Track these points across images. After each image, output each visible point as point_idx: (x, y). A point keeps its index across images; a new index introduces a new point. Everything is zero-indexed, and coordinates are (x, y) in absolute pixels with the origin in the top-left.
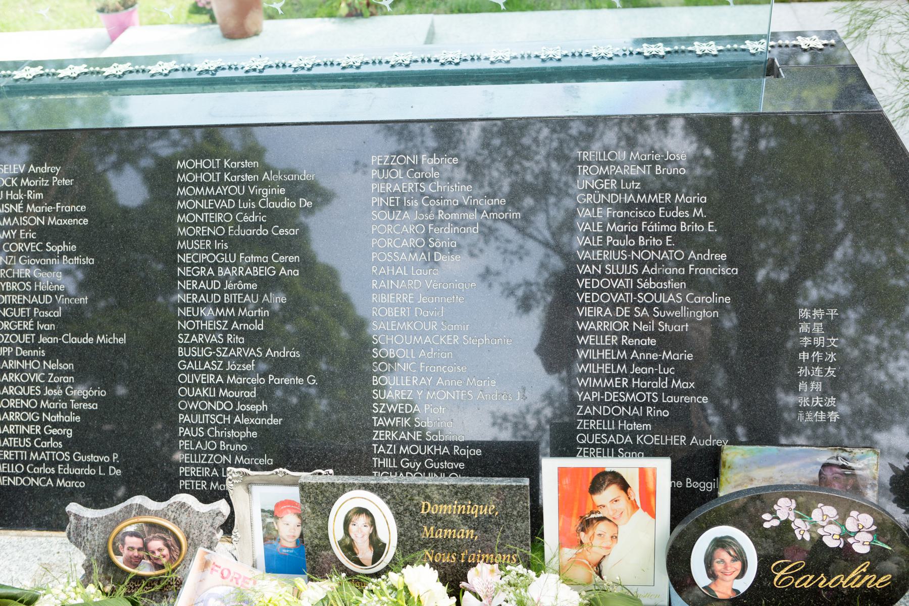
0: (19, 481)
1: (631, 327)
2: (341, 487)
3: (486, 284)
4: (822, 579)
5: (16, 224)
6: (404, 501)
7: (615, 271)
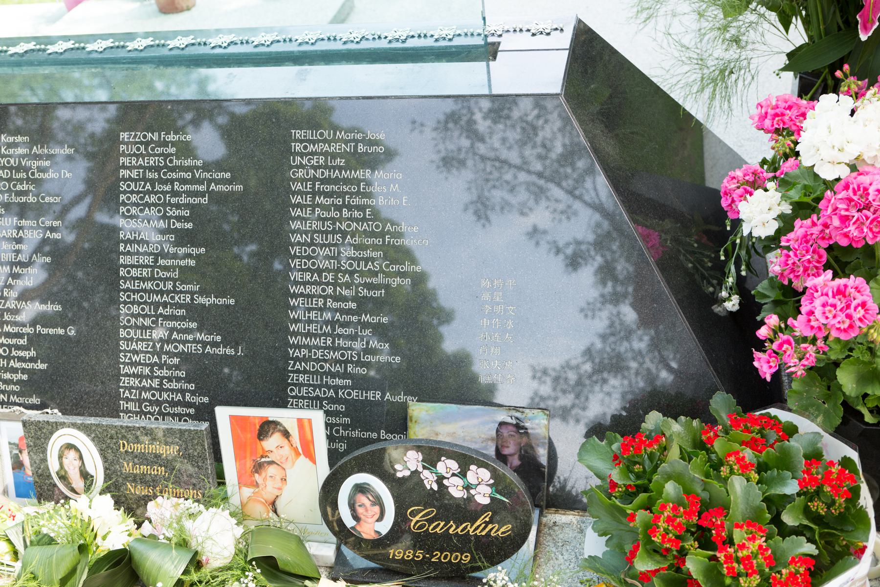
1: (335, 291)
2: (54, 425)
3: (533, 242)
4: (451, 526)
6: (106, 439)
7: (322, 240)
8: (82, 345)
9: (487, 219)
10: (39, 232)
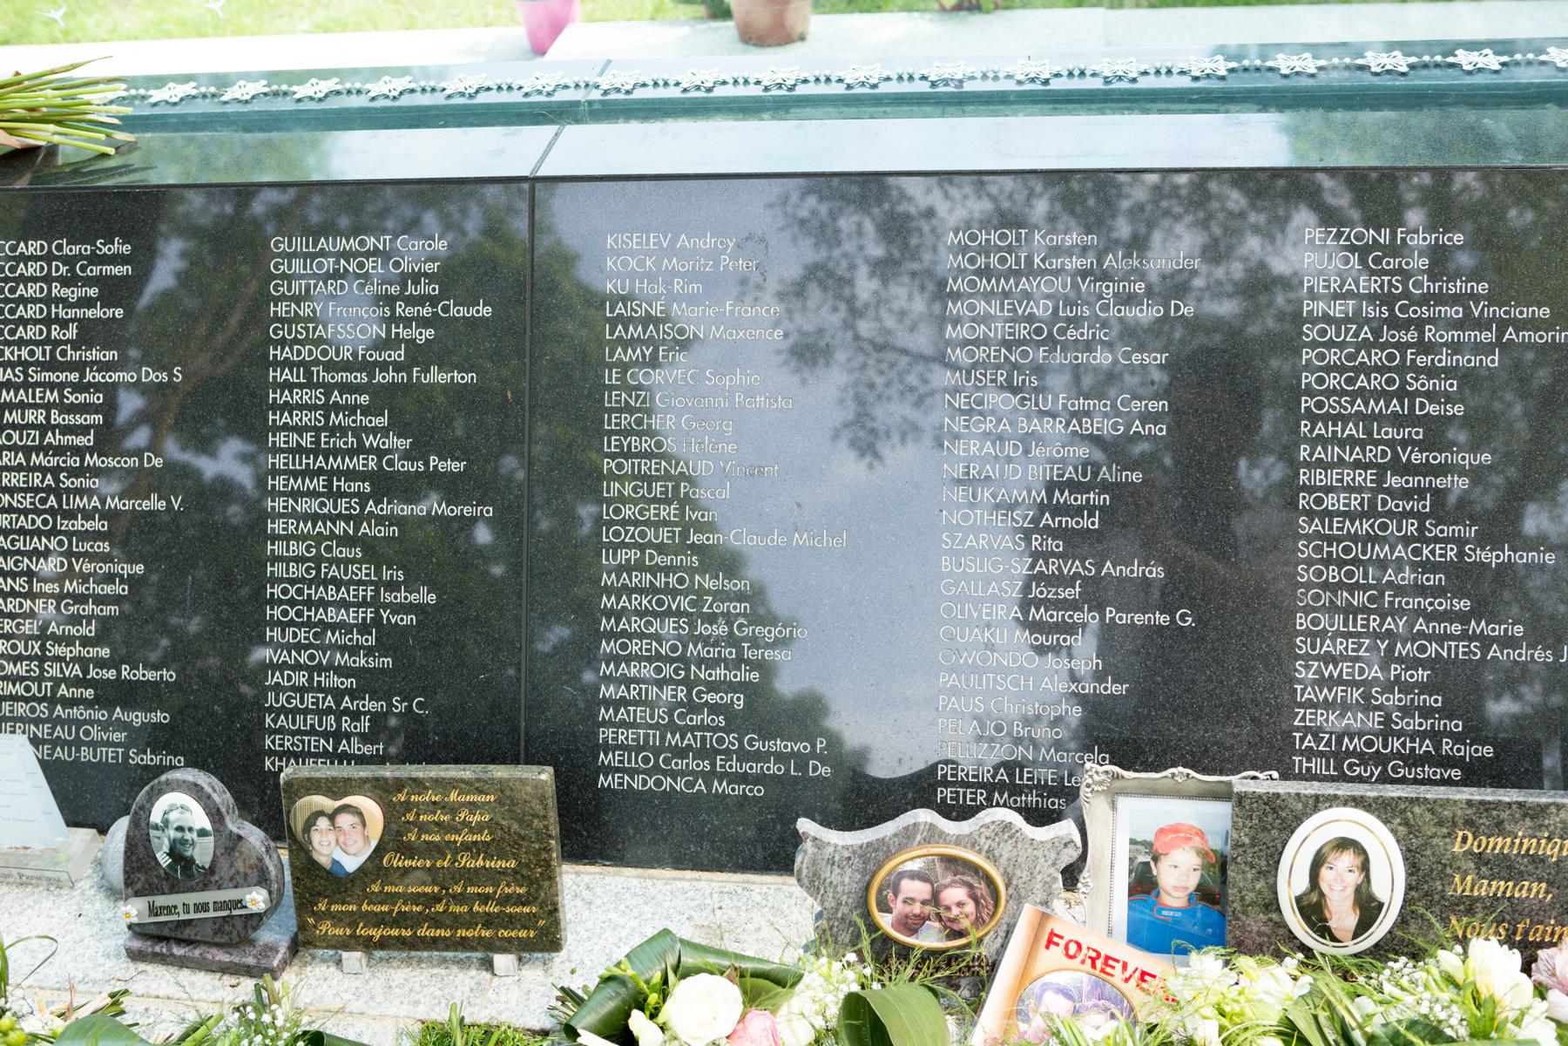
0: (645, 782)
2: (1311, 801)
5: (651, 337)
8: (1210, 646)
9: (877, 455)
10: (1116, 423)
